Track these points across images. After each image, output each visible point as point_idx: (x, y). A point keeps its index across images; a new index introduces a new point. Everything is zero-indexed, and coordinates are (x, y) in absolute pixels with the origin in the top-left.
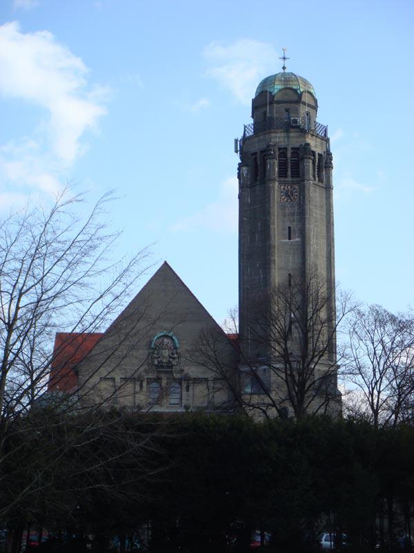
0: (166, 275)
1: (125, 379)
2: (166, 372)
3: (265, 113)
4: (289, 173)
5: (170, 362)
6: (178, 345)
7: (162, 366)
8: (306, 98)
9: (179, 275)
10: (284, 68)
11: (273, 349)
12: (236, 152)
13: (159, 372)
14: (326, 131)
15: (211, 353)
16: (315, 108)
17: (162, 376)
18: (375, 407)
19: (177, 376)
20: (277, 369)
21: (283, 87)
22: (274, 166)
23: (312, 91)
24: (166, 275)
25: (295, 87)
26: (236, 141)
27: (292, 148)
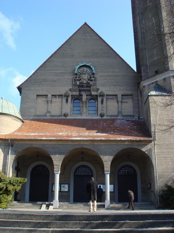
2: (86, 91)
5: (88, 83)
6: (94, 72)
7: (82, 86)
19: (94, 93)
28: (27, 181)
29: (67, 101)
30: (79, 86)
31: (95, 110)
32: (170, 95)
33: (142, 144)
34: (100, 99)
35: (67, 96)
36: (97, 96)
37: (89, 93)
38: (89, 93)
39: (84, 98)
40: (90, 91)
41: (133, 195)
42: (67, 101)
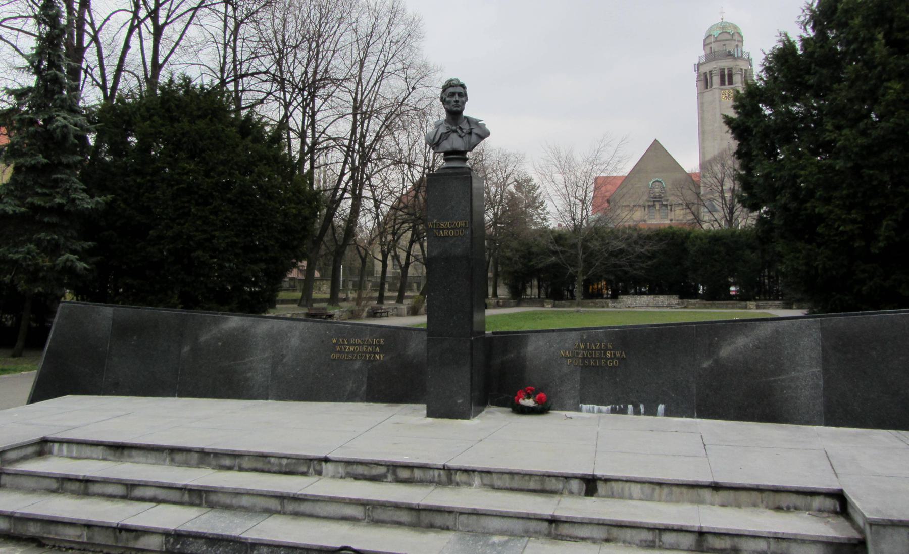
0: (656, 148)
1: (634, 206)
2: (659, 201)
3: (711, 48)
4: (727, 83)
5: (660, 195)
6: (664, 186)
7: (656, 198)
8: (736, 37)
9: (683, 167)
10: (722, 19)
11: (381, 218)
12: (695, 71)
13: (654, 201)
14: (749, 55)
15: (578, 217)
16: (742, 42)
17: (656, 203)
18: (227, 41)
19: (664, 203)
20: (168, 17)
21: (721, 31)
22: (716, 80)
23: (739, 31)
24: (656, 148)
25: (728, 31)
26: (695, 65)
27: (728, 68)
28: (873, 121)
29: (645, 209)
30: (653, 198)
31: (764, 53)
32: (613, 260)
33: (267, 315)
34: (669, 207)
35: (645, 207)
36: (667, 205)
37: (660, 203)
38: (660, 203)
39: (657, 207)
40: (662, 201)
41: (151, 60)
42: (645, 209)
